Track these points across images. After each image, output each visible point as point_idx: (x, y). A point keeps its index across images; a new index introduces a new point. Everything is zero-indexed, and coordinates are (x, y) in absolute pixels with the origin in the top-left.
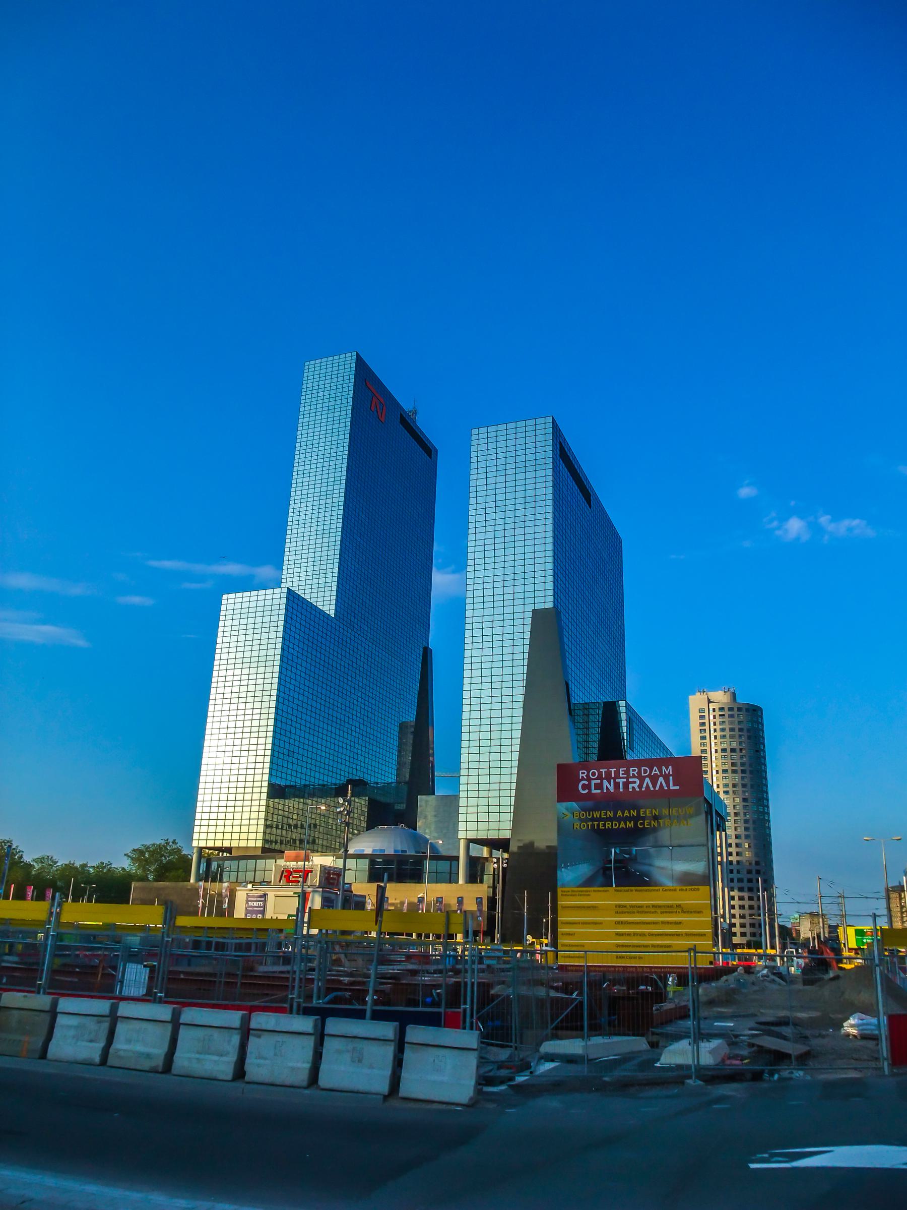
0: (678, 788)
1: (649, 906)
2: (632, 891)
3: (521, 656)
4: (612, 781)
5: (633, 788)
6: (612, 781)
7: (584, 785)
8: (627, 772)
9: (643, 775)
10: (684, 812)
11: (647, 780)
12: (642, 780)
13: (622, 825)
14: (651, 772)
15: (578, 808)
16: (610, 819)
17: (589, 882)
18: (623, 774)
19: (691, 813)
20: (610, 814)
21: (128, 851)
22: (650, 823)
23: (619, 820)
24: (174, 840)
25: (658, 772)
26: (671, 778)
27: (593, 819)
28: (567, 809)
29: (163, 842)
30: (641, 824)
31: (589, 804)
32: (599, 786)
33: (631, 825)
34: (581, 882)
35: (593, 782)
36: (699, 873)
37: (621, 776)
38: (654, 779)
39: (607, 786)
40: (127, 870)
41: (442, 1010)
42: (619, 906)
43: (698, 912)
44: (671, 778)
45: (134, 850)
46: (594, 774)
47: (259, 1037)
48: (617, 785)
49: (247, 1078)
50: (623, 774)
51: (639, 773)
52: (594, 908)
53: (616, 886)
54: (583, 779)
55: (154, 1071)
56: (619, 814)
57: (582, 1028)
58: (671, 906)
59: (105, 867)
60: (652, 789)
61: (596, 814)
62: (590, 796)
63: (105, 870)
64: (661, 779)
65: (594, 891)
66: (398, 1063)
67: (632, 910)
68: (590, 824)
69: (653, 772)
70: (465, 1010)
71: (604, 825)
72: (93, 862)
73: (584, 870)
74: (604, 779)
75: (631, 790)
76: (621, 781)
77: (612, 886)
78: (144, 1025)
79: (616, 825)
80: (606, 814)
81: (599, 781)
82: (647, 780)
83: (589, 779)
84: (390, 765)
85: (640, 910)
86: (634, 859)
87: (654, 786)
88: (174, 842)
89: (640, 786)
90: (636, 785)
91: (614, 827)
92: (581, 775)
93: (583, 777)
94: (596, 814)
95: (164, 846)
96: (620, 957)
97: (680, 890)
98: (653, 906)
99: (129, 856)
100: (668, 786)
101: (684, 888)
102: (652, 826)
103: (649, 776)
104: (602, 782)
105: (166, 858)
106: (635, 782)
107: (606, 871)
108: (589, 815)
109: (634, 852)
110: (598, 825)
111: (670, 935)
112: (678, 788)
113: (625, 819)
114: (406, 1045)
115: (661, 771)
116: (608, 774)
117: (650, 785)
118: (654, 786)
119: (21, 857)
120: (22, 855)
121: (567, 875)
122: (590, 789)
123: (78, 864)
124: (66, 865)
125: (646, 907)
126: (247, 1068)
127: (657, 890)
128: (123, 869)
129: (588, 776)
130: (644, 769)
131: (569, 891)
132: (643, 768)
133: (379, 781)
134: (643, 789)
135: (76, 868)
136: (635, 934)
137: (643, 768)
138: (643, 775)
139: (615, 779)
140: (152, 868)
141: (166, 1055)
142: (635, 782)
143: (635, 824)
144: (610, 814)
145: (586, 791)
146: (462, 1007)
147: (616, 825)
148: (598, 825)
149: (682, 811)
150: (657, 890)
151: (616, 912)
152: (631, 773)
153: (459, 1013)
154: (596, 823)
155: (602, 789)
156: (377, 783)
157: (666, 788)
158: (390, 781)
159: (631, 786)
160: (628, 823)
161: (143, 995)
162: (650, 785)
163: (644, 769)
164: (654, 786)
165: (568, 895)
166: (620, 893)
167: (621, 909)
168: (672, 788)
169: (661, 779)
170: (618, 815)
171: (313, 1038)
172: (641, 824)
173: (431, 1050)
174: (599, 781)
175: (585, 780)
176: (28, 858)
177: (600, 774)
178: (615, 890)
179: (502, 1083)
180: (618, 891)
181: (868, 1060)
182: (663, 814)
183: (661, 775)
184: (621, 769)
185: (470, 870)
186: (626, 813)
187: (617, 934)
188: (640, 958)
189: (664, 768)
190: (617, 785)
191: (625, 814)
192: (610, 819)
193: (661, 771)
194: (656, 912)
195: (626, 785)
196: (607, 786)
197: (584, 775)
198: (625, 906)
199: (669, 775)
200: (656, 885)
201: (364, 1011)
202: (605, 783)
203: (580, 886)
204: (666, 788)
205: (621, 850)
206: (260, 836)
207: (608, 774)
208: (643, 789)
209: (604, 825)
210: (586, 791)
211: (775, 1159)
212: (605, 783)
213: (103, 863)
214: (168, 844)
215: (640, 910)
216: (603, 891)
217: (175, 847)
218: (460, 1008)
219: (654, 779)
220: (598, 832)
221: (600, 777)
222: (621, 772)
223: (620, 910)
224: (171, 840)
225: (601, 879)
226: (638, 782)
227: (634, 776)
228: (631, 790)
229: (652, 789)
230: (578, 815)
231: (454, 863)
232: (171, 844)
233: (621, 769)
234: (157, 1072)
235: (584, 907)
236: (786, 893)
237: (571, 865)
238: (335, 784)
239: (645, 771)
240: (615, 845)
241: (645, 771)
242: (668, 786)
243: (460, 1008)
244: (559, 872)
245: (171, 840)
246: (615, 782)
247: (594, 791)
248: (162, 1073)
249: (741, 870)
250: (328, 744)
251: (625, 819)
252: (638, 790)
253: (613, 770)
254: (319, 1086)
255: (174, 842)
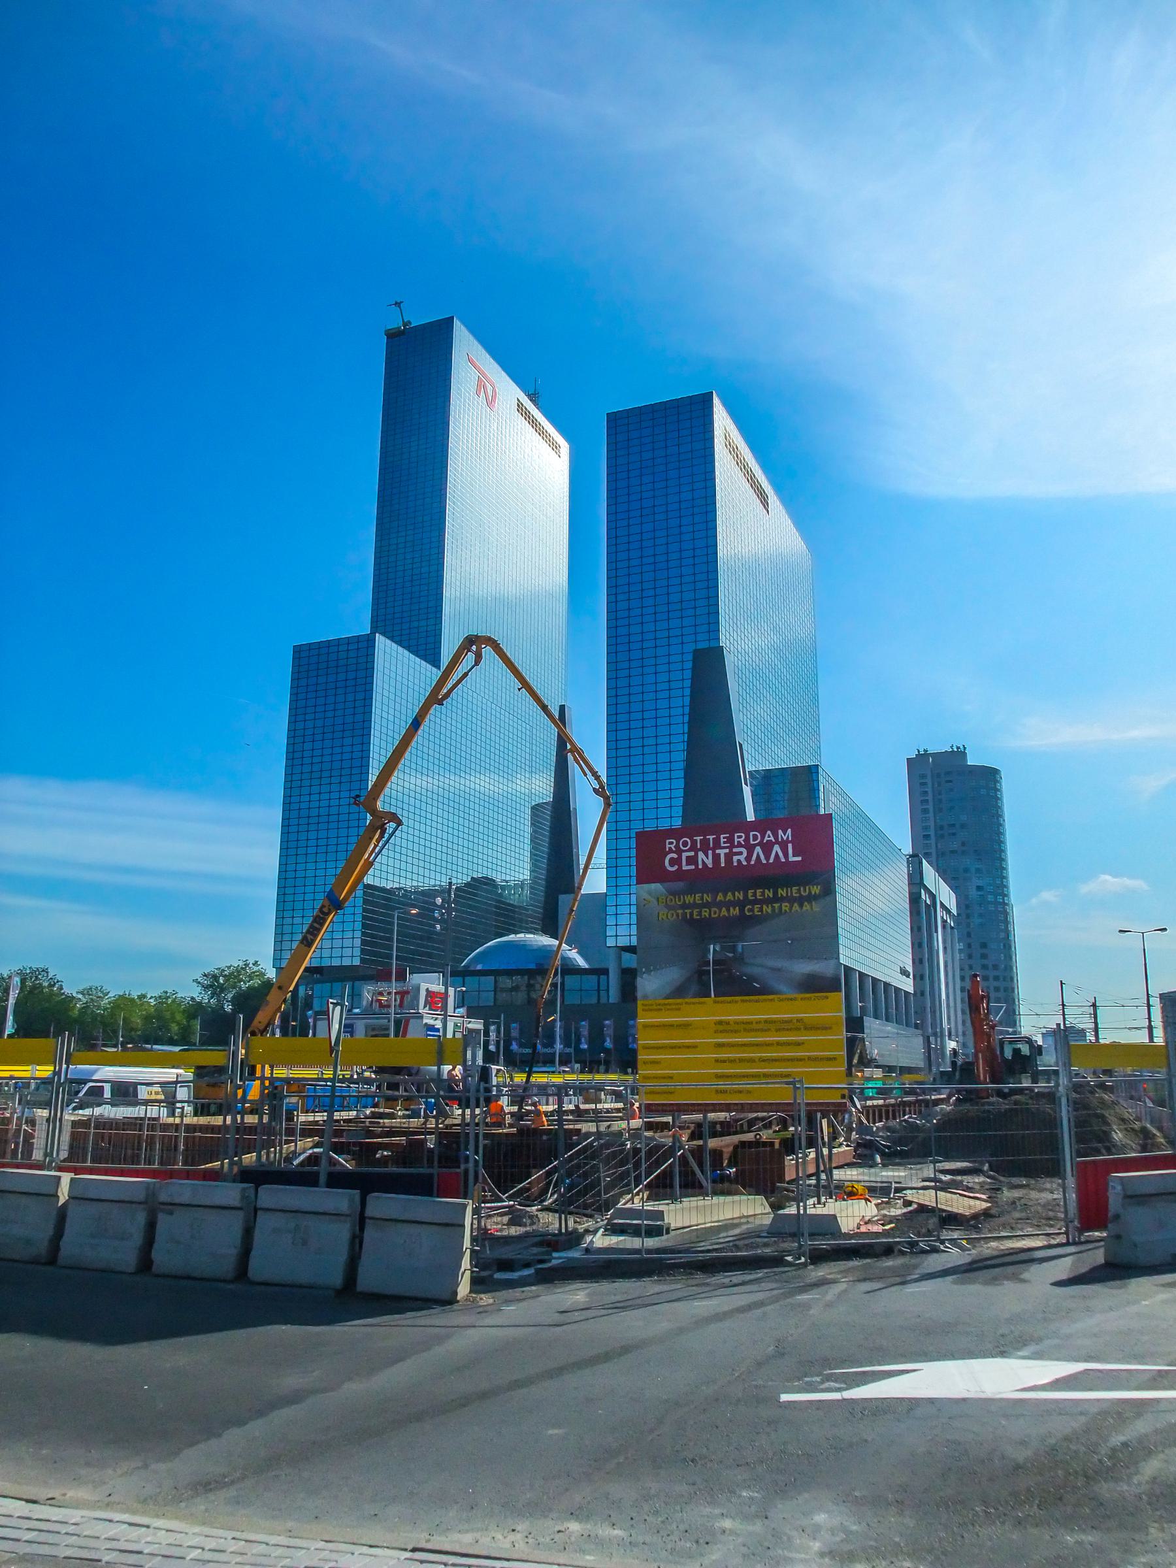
0: (799, 859)
1: (760, 1022)
2: (736, 1002)
3: (680, 711)
4: (710, 852)
5: (739, 861)
6: (710, 852)
7: (672, 859)
8: (730, 840)
9: (752, 842)
10: (807, 890)
11: (758, 849)
12: (750, 849)
13: (724, 912)
14: (763, 838)
15: (664, 890)
16: (707, 905)
17: (679, 992)
18: (724, 843)
19: (817, 892)
20: (708, 898)
21: (198, 976)
22: (762, 908)
23: (720, 905)
24: (256, 962)
25: (772, 838)
26: (790, 846)
27: (684, 906)
28: (650, 893)
29: (241, 963)
30: (749, 910)
31: (679, 885)
32: (692, 860)
33: (735, 911)
34: (668, 992)
35: (684, 855)
36: (829, 975)
37: (723, 845)
38: (767, 848)
39: (703, 860)
40: (198, 1000)
41: (435, 1171)
42: (720, 1023)
43: (826, 1028)
44: (790, 846)
45: (205, 975)
46: (685, 844)
47: (171, 1213)
48: (716, 858)
49: (154, 1269)
50: (724, 843)
51: (747, 839)
52: (685, 1026)
53: (715, 996)
54: (671, 851)
55: (35, 1261)
56: (720, 897)
57: (672, 1186)
58: (789, 1021)
59: (169, 997)
60: (764, 862)
61: (689, 899)
62: (680, 875)
63: (170, 1001)
64: (777, 848)
65: (686, 1003)
66: (357, 1242)
67: (736, 1027)
68: (680, 912)
69: (766, 838)
70: (466, 1172)
71: (700, 914)
72: (153, 993)
73: (672, 975)
74: (700, 850)
75: (735, 864)
76: (722, 852)
77: (710, 996)
78: (24, 1200)
79: (715, 913)
80: (702, 898)
81: (692, 854)
82: (758, 849)
83: (679, 851)
84: (521, 858)
85: (747, 1027)
86: (740, 959)
87: (767, 857)
88: (256, 964)
89: (748, 858)
90: (742, 858)
91: (713, 916)
92: (668, 846)
93: (670, 848)
94: (689, 899)
95: (242, 968)
96: (721, 1092)
97: (801, 999)
98: (766, 1021)
99: (199, 983)
100: (786, 855)
101: (808, 995)
102: (764, 912)
103: (760, 844)
104: (696, 854)
105: (245, 984)
106: (741, 853)
107: (700, 975)
108: (680, 900)
109: (740, 949)
110: (691, 914)
111: (788, 1060)
112: (799, 859)
113: (729, 905)
114: (367, 1220)
115: (776, 836)
116: (705, 843)
117: (781, 854)
118: (767, 857)
119: (61, 988)
120: (61, 985)
121: (649, 984)
122: (680, 865)
123: (135, 995)
124: (120, 996)
125: (757, 1023)
126: (155, 1255)
127: (771, 1000)
128: (193, 998)
129: (677, 846)
130: (753, 835)
131: (652, 1005)
132: (751, 833)
133: (508, 878)
134: (752, 863)
135: (133, 999)
136: (741, 1060)
137: (751, 833)
138: (752, 842)
139: (714, 850)
140: (230, 996)
141: (51, 1241)
142: (741, 853)
143: (742, 910)
144: (708, 898)
145: (676, 867)
146: (463, 1166)
147: (715, 913)
148: (691, 914)
149: (805, 890)
150: (771, 1000)
151: (716, 1032)
152: (736, 840)
153: (457, 1174)
154: (688, 911)
155: (696, 864)
156: (507, 882)
157: (783, 860)
158: (521, 877)
159: (735, 858)
160: (731, 909)
161: (64, 1161)
162: (762, 857)
163: (753, 835)
164: (767, 858)
165: (651, 1010)
166: (721, 1005)
167: (723, 1027)
168: (792, 859)
169: (777, 848)
170: (719, 898)
171: (241, 1214)
172: (749, 910)
173: (399, 1225)
174: (692, 854)
175: (673, 852)
176: (70, 989)
177: (694, 843)
178: (715, 1002)
179: (527, 1265)
180: (718, 1002)
181: (681, 1331)
182: (741, 892)
183: (777, 842)
184: (722, 836)
185: (1012, 979)
186: (730, 896)
187: (717, 1061)
188: (749, 1092)
189: (780, 832)
190: (716, 858)
191: (728, 898)
192: (707, 905)
193: (776, 836)
194: (769, 1030)
195: (729, 857)
196: (703, 860)
197: (672, 846)
198: (728, 1023)
199: (788, 841)
200: (772, 993)
201: (317, 1174)
202: (701, 855)
203: (667, 997)
204: (783, 860)
205: (722, 948)
206: (357, 952)
207: (705, 843)
208: (752, 863)
209: (700, 914)
210: (676, 867)
211: (827, 1385)
212: (701, 855)
213: (166, 992)
214: (247, 965)
215: (747, 1027)
216: (699, 1003)
217: (255, 969)
218: (459, 1167)
219: (767, 848)
220: (691, 922)
221: (693, 848)
222: (722, 840)
223: (721, 1028)
224: (251, 961)
225: (694, 988)
226: (745, 854)
227: (739, 845)
228: (735, 864)
229: (764, 862)
230: (664, 901)
231: (603, 977)
232: (251, 965)
233: (722, 836)
234: (38, 1263)
235: (672, 1026)
236: (1078, 992)
237: (655, 969)
238: (440, 886)
239: (755, 838)
240: (714, 940)
241: (755, 838)
242: (786, 855)
243: (459, 1167)
244: (639, 979)
245: (251, 961)
246: (714, 854)
247: (685, 868)
248: (45, 1264)
249: (974, 966)
250: (440, 833)
251: (729, 905)
252: (745, 863)
253: (711, 837)
254: (248, 1278)
255: (256, 964)
